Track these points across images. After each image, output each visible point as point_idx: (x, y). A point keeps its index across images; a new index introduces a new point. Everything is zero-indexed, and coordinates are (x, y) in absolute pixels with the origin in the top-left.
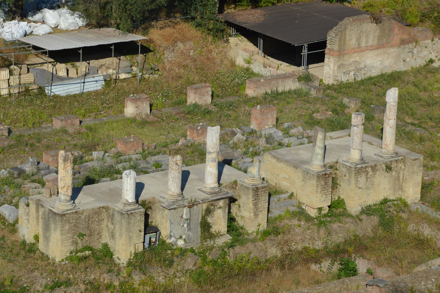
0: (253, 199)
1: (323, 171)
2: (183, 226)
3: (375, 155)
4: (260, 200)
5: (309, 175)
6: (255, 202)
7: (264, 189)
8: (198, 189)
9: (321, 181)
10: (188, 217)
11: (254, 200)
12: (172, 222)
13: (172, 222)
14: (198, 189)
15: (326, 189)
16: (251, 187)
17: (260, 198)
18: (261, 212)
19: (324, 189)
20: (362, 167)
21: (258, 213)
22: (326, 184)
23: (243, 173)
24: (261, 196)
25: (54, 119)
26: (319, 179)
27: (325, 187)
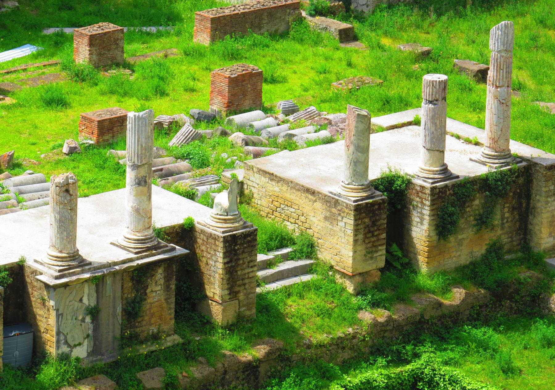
0: (226, 260)
1: (367, 198)
2: (83, 320)
3: (471, 160)
4: (241, 262)
5: (339, 208)
6: (232, 266)
7: (249, 238)
8: (111, 243)
9: (364, 218)
10: (93, 303)
11: (228, 263)
12: (60, 312)
13: (60, 312)
14: (111, 243)
15: (376, 233)
16: (428, 185)
17: (241, 257)
18: (242, 288)
19: (370, 235)
20: (446, 186)
21: (237, 289)
22: (374, 224)
23: (474, 146)
24: (243, 252)
25: (302, 11)
26: (361, 213)
27: (372, 229)
